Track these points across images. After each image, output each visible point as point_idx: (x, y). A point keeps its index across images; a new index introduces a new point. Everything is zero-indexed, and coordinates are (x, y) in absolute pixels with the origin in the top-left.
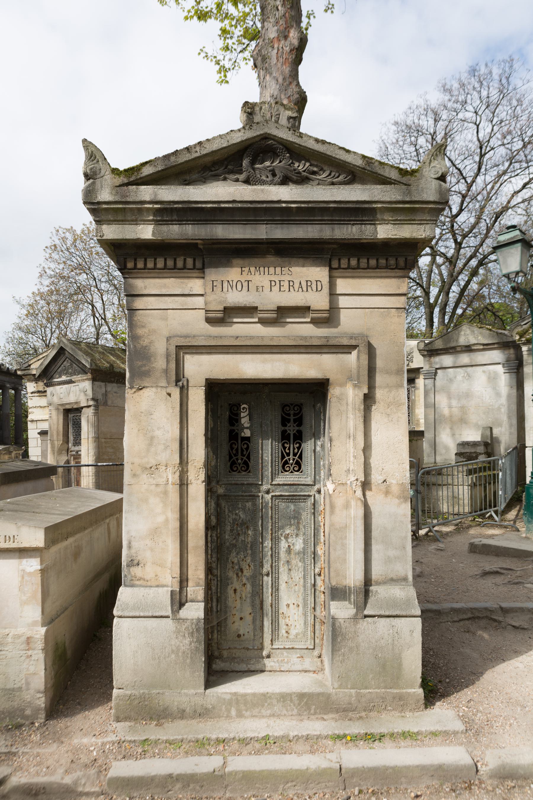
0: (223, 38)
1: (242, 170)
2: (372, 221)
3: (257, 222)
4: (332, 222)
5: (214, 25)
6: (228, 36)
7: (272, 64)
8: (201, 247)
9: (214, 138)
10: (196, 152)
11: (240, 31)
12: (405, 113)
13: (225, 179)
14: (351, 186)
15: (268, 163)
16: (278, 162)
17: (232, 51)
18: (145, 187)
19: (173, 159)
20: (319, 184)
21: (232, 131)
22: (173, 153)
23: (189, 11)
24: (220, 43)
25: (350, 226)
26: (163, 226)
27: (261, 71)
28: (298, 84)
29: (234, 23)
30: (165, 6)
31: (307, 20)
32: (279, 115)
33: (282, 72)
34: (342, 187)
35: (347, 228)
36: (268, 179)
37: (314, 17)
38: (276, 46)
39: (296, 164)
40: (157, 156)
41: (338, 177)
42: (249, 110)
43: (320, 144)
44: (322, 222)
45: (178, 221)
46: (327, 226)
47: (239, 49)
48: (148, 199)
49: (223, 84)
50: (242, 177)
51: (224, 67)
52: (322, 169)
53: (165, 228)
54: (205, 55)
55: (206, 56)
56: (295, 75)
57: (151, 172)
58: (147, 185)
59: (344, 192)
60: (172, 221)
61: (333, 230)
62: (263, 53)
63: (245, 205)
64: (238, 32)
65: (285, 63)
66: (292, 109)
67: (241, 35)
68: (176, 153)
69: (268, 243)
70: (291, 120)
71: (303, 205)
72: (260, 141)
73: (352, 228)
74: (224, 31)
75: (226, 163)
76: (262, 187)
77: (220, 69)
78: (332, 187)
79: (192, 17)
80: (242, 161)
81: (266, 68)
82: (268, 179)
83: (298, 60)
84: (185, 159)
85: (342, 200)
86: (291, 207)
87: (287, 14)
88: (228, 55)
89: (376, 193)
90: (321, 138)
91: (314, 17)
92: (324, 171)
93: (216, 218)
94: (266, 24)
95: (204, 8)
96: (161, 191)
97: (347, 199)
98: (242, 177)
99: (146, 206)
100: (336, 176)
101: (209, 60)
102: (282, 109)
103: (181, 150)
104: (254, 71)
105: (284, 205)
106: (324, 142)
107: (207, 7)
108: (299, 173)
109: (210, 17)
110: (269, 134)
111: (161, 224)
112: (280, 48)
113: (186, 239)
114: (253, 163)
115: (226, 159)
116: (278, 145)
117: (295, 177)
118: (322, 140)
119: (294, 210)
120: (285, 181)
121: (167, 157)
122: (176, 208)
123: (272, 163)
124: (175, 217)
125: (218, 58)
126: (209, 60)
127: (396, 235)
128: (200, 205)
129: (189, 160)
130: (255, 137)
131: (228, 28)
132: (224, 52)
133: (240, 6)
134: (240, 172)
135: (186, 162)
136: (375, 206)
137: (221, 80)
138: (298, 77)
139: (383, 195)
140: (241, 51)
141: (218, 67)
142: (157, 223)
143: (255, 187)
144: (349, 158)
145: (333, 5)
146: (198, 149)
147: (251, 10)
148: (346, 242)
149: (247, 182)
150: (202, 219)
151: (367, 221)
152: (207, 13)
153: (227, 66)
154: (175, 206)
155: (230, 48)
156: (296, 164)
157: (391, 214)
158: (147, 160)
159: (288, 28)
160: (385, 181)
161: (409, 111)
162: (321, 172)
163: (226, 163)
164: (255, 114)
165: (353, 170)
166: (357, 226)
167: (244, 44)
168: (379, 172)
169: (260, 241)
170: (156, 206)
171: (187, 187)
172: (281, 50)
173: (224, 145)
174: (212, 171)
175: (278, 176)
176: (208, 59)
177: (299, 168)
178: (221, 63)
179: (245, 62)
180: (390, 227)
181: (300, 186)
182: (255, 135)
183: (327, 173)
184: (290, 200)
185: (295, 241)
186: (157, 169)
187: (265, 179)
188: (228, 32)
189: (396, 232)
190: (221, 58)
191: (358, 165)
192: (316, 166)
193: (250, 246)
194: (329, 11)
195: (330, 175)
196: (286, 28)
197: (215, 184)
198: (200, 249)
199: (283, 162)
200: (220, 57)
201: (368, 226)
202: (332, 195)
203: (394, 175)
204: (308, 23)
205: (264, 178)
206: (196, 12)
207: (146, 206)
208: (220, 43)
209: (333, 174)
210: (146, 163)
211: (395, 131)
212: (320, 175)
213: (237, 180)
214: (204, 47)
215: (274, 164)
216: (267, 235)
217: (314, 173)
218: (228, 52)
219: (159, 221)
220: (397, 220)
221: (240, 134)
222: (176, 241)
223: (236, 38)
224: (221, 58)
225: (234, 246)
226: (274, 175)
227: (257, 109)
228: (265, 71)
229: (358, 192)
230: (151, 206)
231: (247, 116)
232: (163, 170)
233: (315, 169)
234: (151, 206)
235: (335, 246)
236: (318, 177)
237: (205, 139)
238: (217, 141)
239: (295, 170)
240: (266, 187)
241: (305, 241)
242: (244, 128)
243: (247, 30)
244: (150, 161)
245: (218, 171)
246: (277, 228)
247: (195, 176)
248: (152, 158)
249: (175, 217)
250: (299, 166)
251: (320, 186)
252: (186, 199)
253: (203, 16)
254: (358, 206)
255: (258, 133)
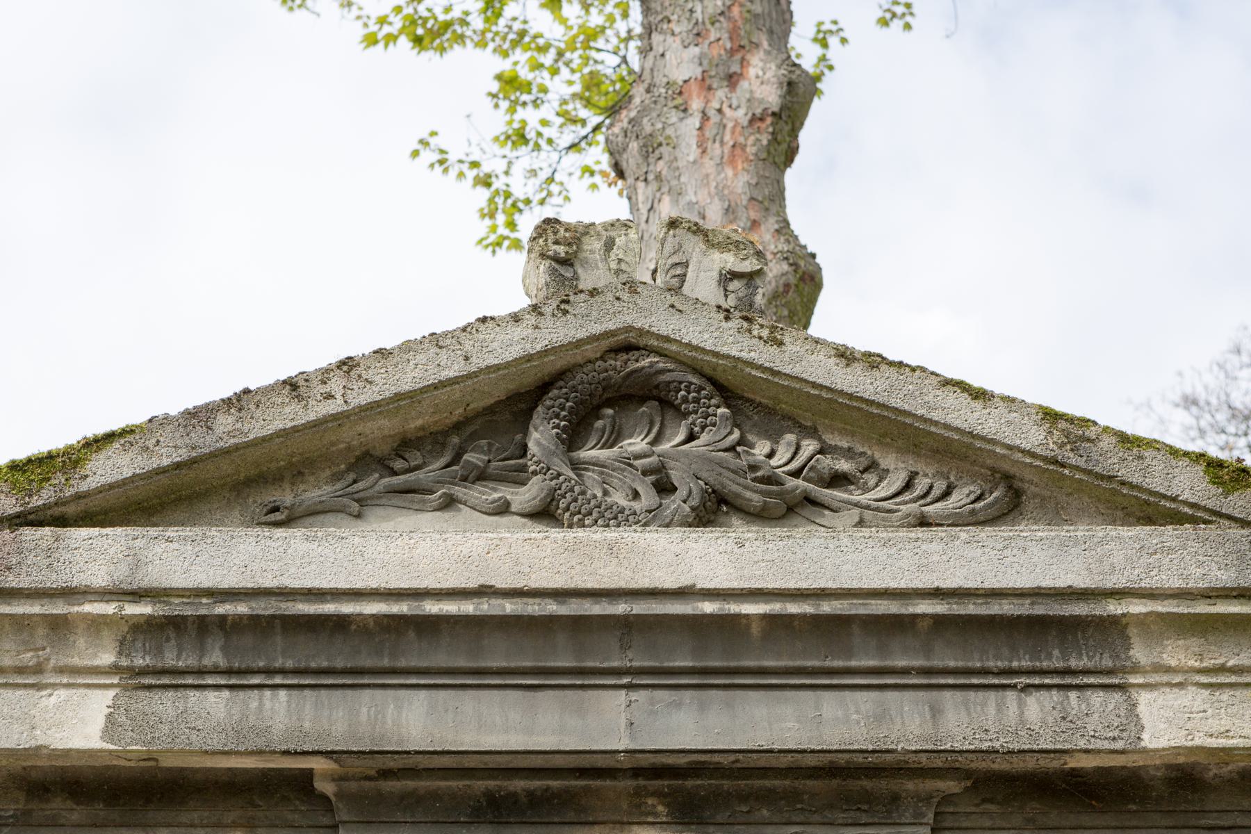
0: (504, 105)
1: (524, 468)
2: (1109, 672)
3: (584, 678)
4: (931, 679)
5: (475, 67)
6: (525, 97)
7: (681, 164)
8: (325, 787)
9: (407, 347)
10: (330, 396)
11: (570, 83)
12: (1221, 366)
13: (449, 503)
14: (1004, 531)
15: (636, 443)
16: (681, 437)
17: (537, 147)
18: (95, 531)
19: (224, 422)
20: (861, 523)
21: (484, 320)
22: (227, 402)
23: (383, 21)
24: (497, 121)
25: (1011, 695)
26: (156, 695)
27: (641, 185)
28: (784, 228)
29: (548, 59)
30: (300, 14)
31: (818, 50)
32: (686, 265)
33: (720, 192)
34: (963, 534)
35: (1000, 707)
36: (636, 506)
37: (844, 41)
38: (696, 105)
39: (761, 448)
40: (159, 412)
41: (946, 495)
42: (561, 250)
43: (858, 367)
44: (882, 679)
45: (229, 672)
46: (908, 695)
47: (567, 138)
48: (98, 578)
49: (501, 252)
50: (526, 495)
51: (508, 195)
52: (872, 466)
53: (164, 704)
54: (437, 157)
55: (441, 162)
56: (771, 198)
57: (127, 473)
58: (102, 524)
59: (974, 552)
60: (201, 672)
61: (936, 712)
62: (648, 129)
63: (534, 608)
64: (561, 86)
65: (732, 161)
66: (737, 244)
67: (575, 96)
68: (240, 401)
69: (637, 772)
70: (735, 285)
71: (793, 608)
72: (602, 358)
73: (1021, 705)
74: (510, 84)
75: (455, 440)
76: (612, 534)
77: (491, 200)
78: (920, 532)
79: (391, 39)
80: (526, 433)
81: (658, 177)
82: (636, 506)
83: (782, 150)
84: (278, 425)
85: (970, 584)
86: (738, 616)
87: (736, 11)
88: (524, 158)
89: (1118, 558)
90: (860, 344)
91: (844, 41)
92: (883, 474)
93: (402, 663)
94: (656, 38)
95: (438, 11)
96: (159, 548)
97: (992, 583)
98: (526, 495)
99: (88, 608)
100: (936, 492)
101: (453, 173)
102: (694, 246)
103: (266, 391)
104: (614, 190)
105: (708, 607)
106: (874, 361)
107: (448, 9)
108: (770, 480)
109: (460, 39)
110: (641, 332)
111: (150, 687)
112: (712, 113)
113: (260, 752)
114: (573, 437)
115: (457, 427)
116: (677, 375)
117: (755, 497)
118: (869, 355)
119: (755, 629)
120: (714, 509)
121: (199, 416)
122: (223, 618)
123: (654, 442)
124: (215, 657)
125: (486, 168)
126: (453, 173)
127: (1226, 733)
128: (329, 608)
129: (295, 429)
130: (579, 343)
131: (525, 74)
132: (507, 150)
133: (572, 11)
134: (518, 477)
135: (283, 433)
136: (1114, 608)
137: (493, 238)
138: (782, 206)
139: (1149, 568)
140: (573, 147)
141: (483, 194)
142: (136, 679)
143: (580, 533)
144: (985, 421)
145: (908, 6)
146: (336, 385)
147: (611, 19)
148: (1000, 765)
149: (545, 513)
150: (339, 663)
151: (1087, 672)
152: (447, 25)
153: (519, 192)
154: (220, 609)
155: (531, 135)
156: (761, 448)
157: (1195, 643)
158: (116, 426)
159: (740, 49)
160: (1151, 510)
161: (1235, 359)
162: (871, 479)
163: (455, 440)
164: (585, 263)
165: (1006, 466)
166: (1044, 694)
167: (584, 122)
168: (1122, 473)
169: (601, 762)
170: (132, 609)
171: (279, 532)
172: (715, 118)
173: (450, 374)
174: (394, 473)
175: (682, 492)
176: (446, 170)
177: (774, 462)
178: (498, 184)
179: (588, 181)
180: (1194, 698)
181: (778, 531)
182: (581, 334)
183: (895, 482)
184: (735, 585)
185: (763, 761)
186: (154, 463)
187: (623, 502)
188: (526, 87)
189: (1226, 723)
190: (500, 166)
191: (1025, 445)
192: (849, 453)
193: (555, 784)
194: (897, 24)
195: (908, 486)
196: (732, 52)
197: (406, 521)
198: (325, 798)
199: (704, 438)
200: (493, 164)
201: (1097, 698)
202: (920, 568)
203: (1190, 486)
204: (823, 59)
205: (619, 499)
206: (412, 21)
207: (88, 608)
208: (497, 121)
209: (921, 484)
210: (110, 437)
211: (1188, 429)
212: (866, 490)
213: (503, 509)
214: (434, 134)
215: (665, 446)
216: (632, 737)
217: (838, 480)
218: (524, 150)
219: (144, 672)
220: (1222, 669)
221: (518, 332)
222: (209, 763)
223: (556, 104)
224: (498, 166)
225: (481, 785)
226: (664, 488)
227: (593, 246)
228: (654, 186)
229: (1038, 554)
230: (109, 609)
231: (553, 271)
232: (177, 466)
233: (844, 466)
234: (109, 609)
235: (951, 786)
236: (857, 497)
237: (368, 350)
238: (421, 358)
239: (753, 468)
240: (629, 536)
241: (811, 761)
242: (535, 309)
243: (593, 81)
244: (125, 432)
245: (420, 475)
246: (678, 705)
247: (315, 492)
248: (138, 417)
249: (215, 657)
250: (771, 455)
251: (865, 532)
252: (268, 582)
253: (431, 35)
254: (1039, 610)
255: (597, 329)
